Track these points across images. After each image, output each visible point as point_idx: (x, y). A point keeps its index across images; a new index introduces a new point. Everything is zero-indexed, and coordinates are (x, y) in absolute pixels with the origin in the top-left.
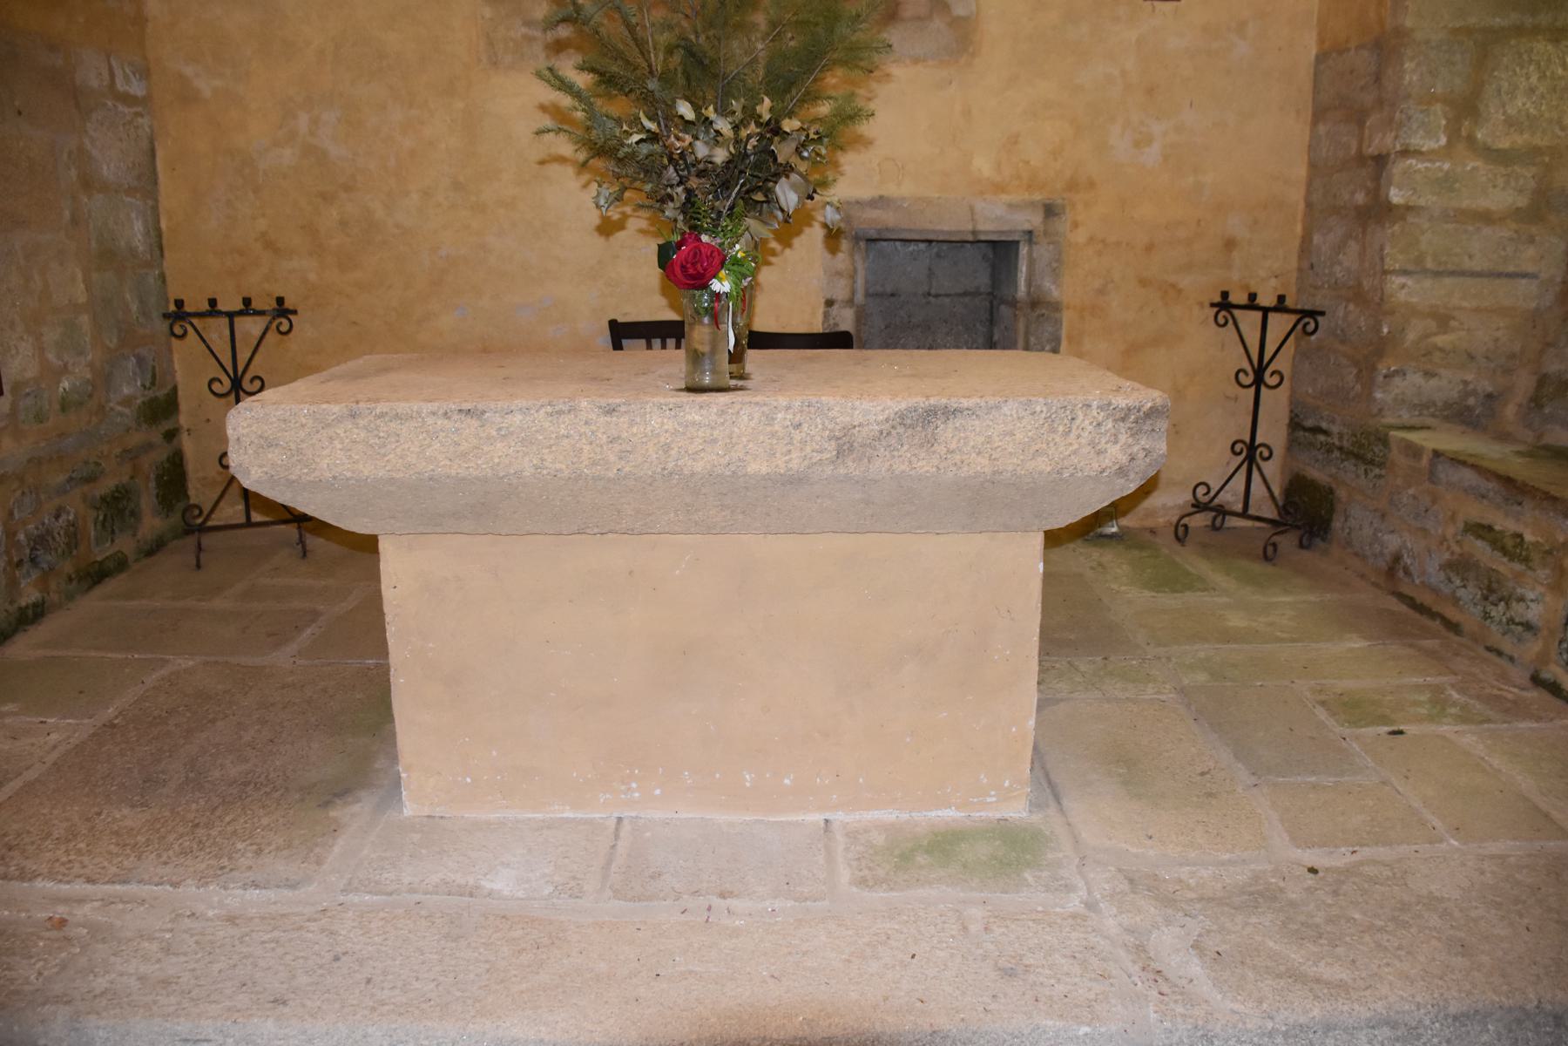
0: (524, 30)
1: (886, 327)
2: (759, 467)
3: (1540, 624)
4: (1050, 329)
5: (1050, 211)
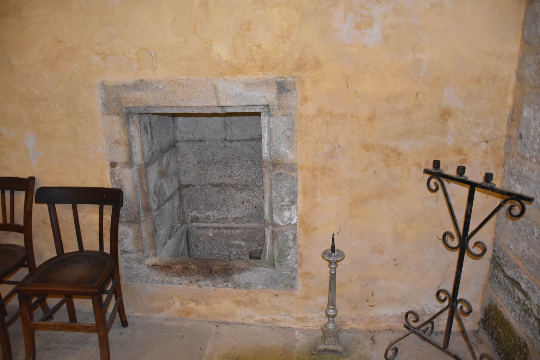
1: (198, 163)
4: (288, 185)
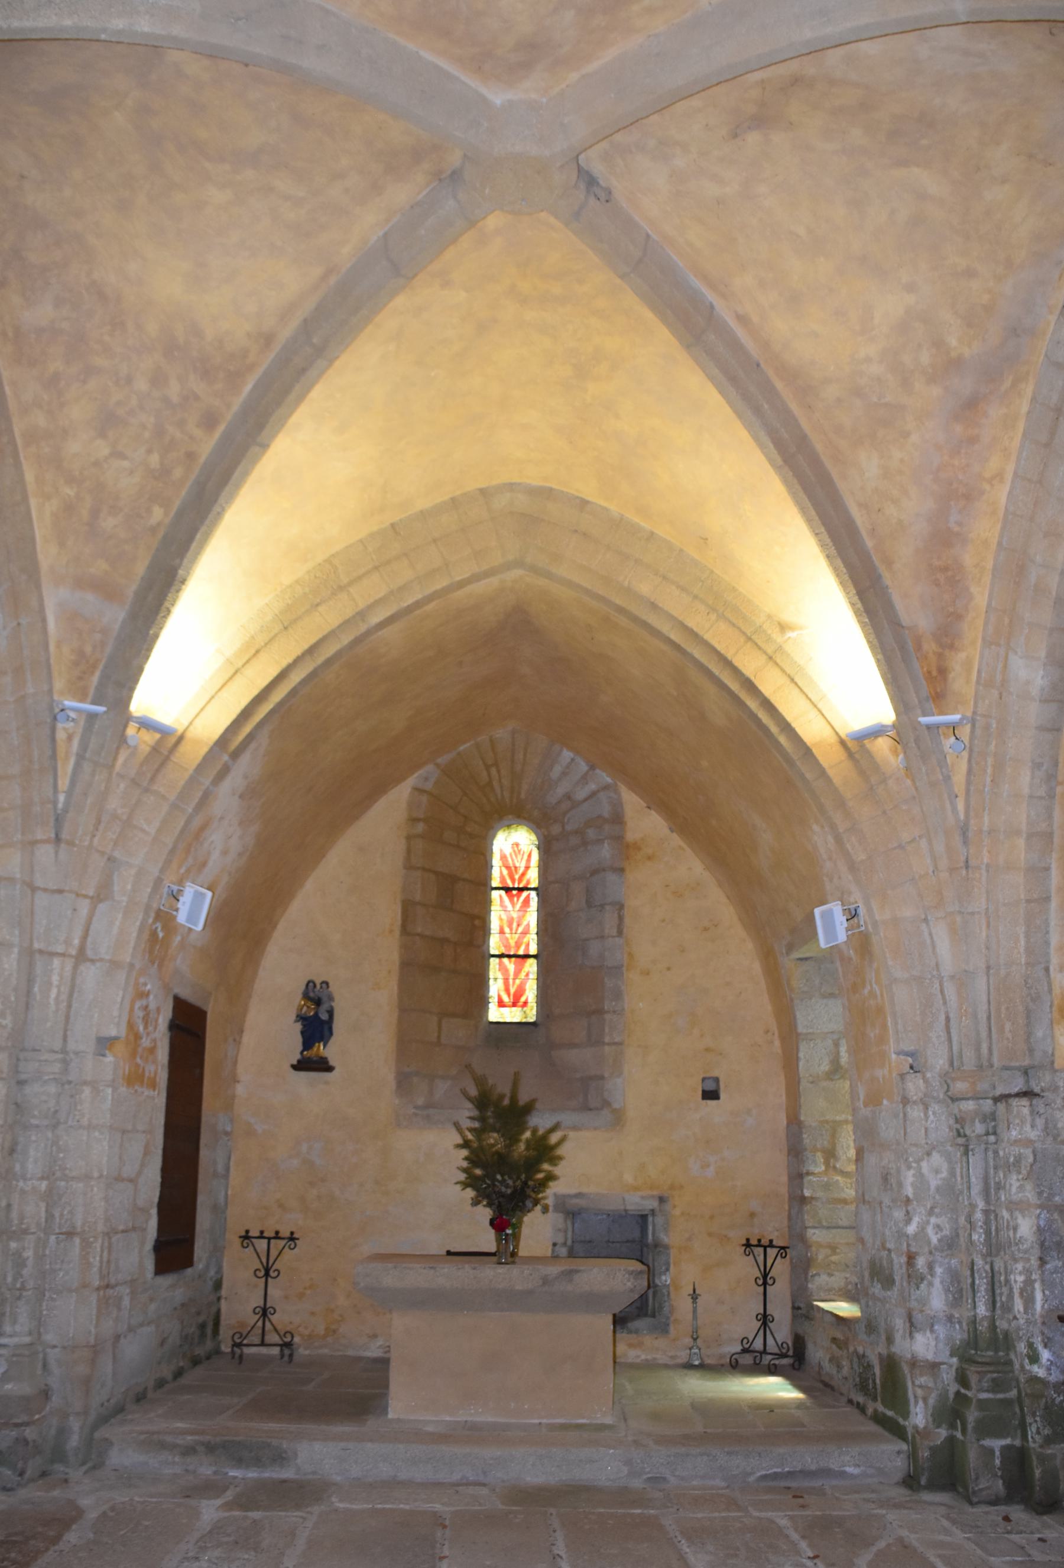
0: (413, 1110)
2: (519, 1287)
3: (681, 1306)
5: (662, 1200)
